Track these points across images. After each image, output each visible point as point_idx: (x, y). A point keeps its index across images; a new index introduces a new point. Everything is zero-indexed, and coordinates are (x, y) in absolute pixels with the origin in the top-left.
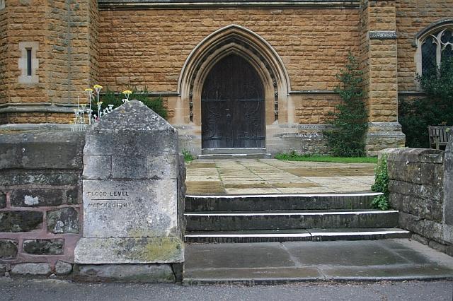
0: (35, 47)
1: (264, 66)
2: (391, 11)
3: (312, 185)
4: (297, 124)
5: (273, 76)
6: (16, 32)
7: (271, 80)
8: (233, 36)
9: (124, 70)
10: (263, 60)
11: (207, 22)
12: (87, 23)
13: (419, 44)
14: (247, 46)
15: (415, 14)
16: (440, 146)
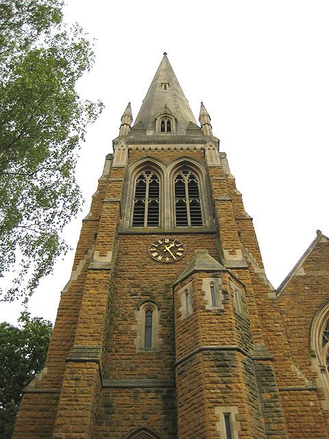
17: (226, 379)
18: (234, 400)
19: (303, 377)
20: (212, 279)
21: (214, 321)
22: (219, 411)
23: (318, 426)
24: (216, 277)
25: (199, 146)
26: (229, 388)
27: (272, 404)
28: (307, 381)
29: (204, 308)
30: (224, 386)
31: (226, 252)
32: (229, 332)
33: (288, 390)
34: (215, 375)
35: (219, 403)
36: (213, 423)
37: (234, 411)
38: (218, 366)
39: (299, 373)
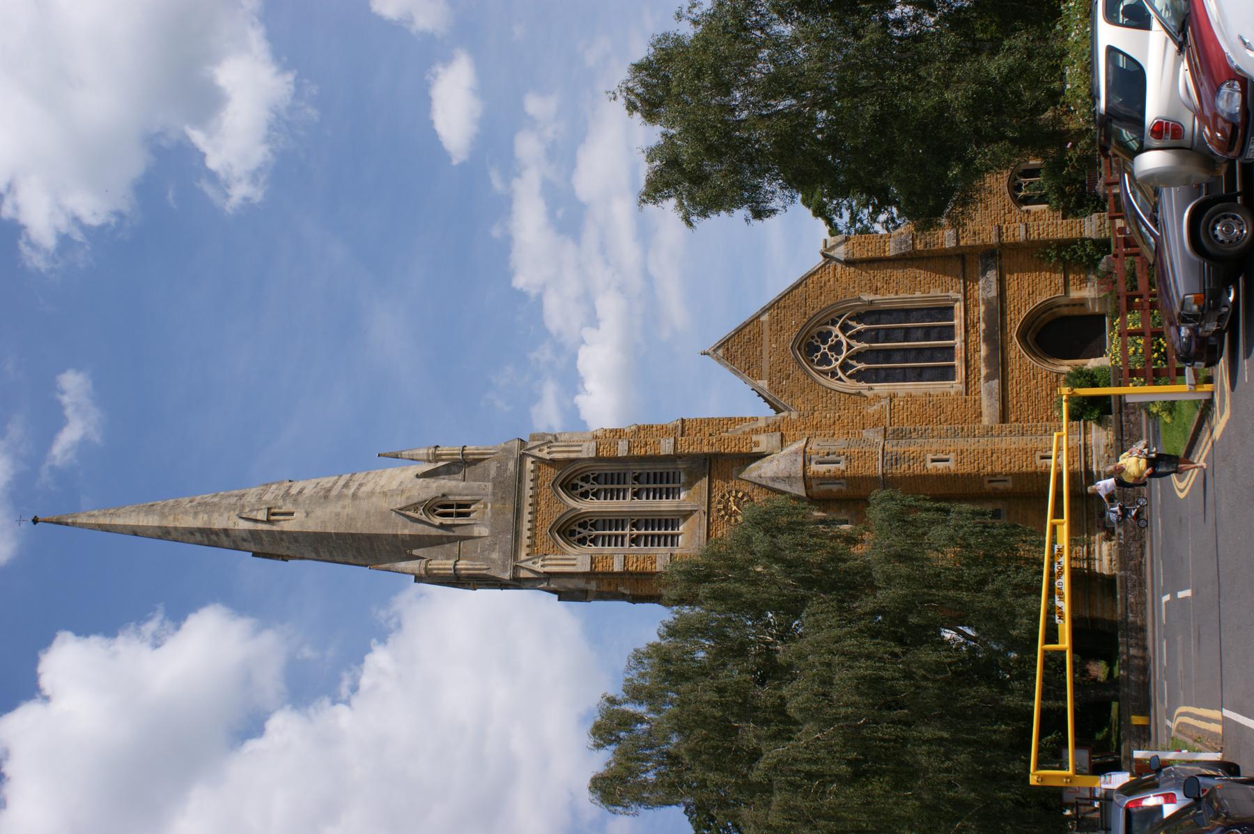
0: (1039, 454)
1: (1044, 315)
2: (1007, 228)
3: (1205, 446)
4: (1088, 289)
5: (1051, 309)
6: (1029, 466)
7: (1054, 310)
8: (1022, 336)
9: (1049, 411)
10: (1039, 317)
11: (1012, 354)
12: (1021, 425)
13: (1024, 208)
14: (1029, 328)
15: (1002, 212)
16: (1155, 302)
17: (906, 460)
18: (922, 455)
19: (879, 405)
20: (813, 463)
21: (856, 464)
22: (930, 465)
23: (918, 402)
24: (810, 460)
25: (529, 465)
26: (913, 459)
27: (920, 432)
28: (883, 403)
29: (843, 471)
30: (912, 461)
31: (755, 450)
32: (867, 454)
33: (891, 418)
34: (903, 466)
35: (924, 465)
36: (938, 470)
37: (930, 456)
38: (896, 464)
39: (875, 407)
